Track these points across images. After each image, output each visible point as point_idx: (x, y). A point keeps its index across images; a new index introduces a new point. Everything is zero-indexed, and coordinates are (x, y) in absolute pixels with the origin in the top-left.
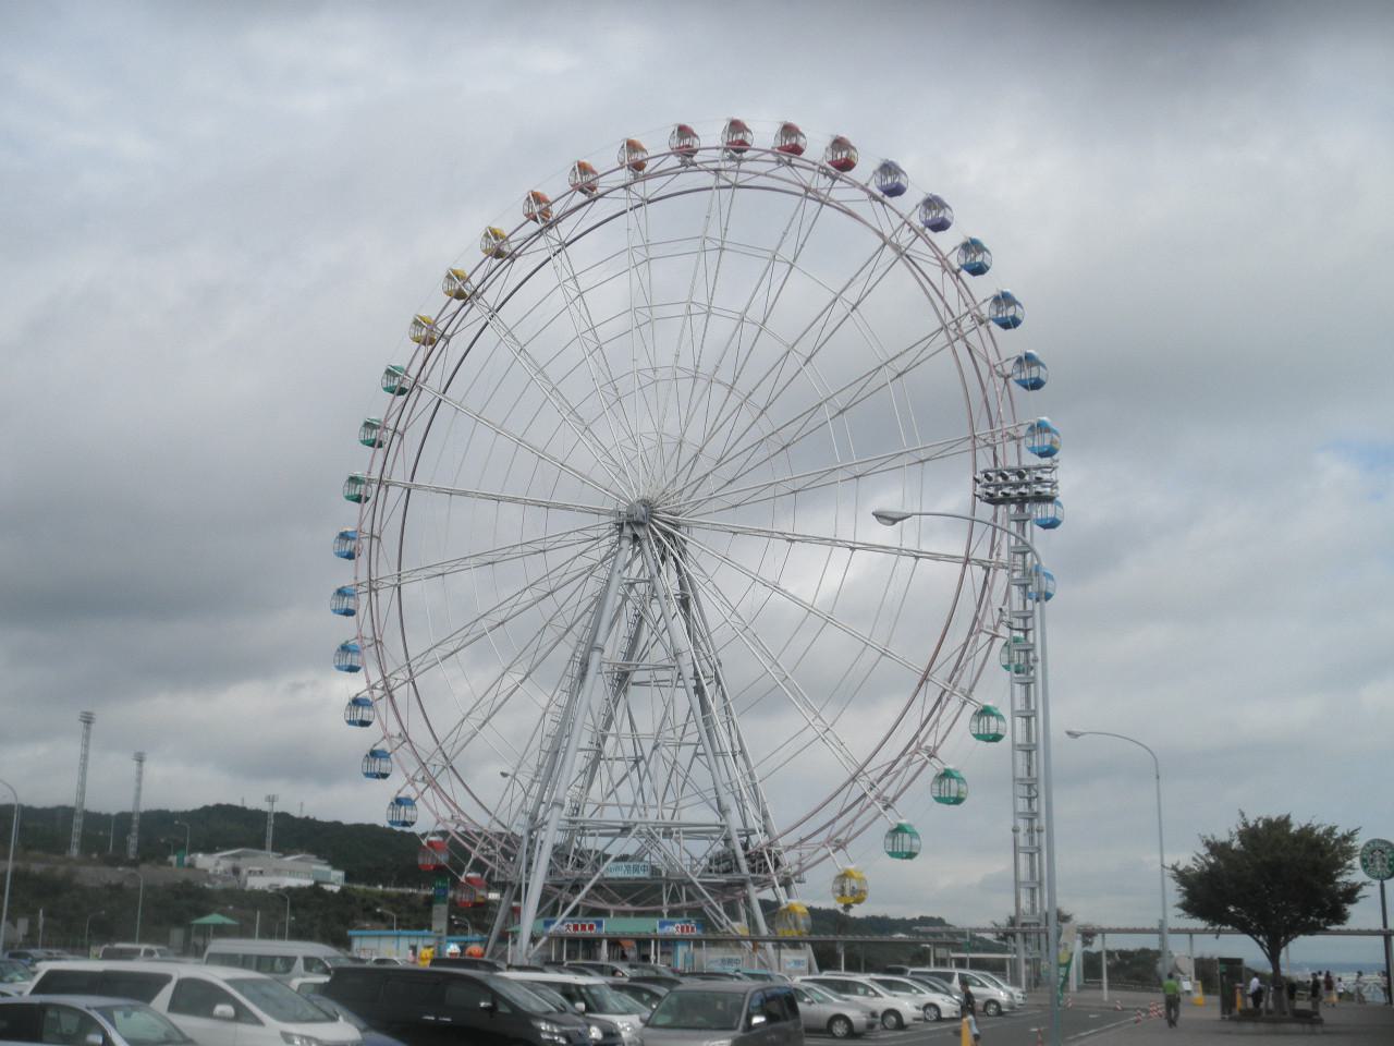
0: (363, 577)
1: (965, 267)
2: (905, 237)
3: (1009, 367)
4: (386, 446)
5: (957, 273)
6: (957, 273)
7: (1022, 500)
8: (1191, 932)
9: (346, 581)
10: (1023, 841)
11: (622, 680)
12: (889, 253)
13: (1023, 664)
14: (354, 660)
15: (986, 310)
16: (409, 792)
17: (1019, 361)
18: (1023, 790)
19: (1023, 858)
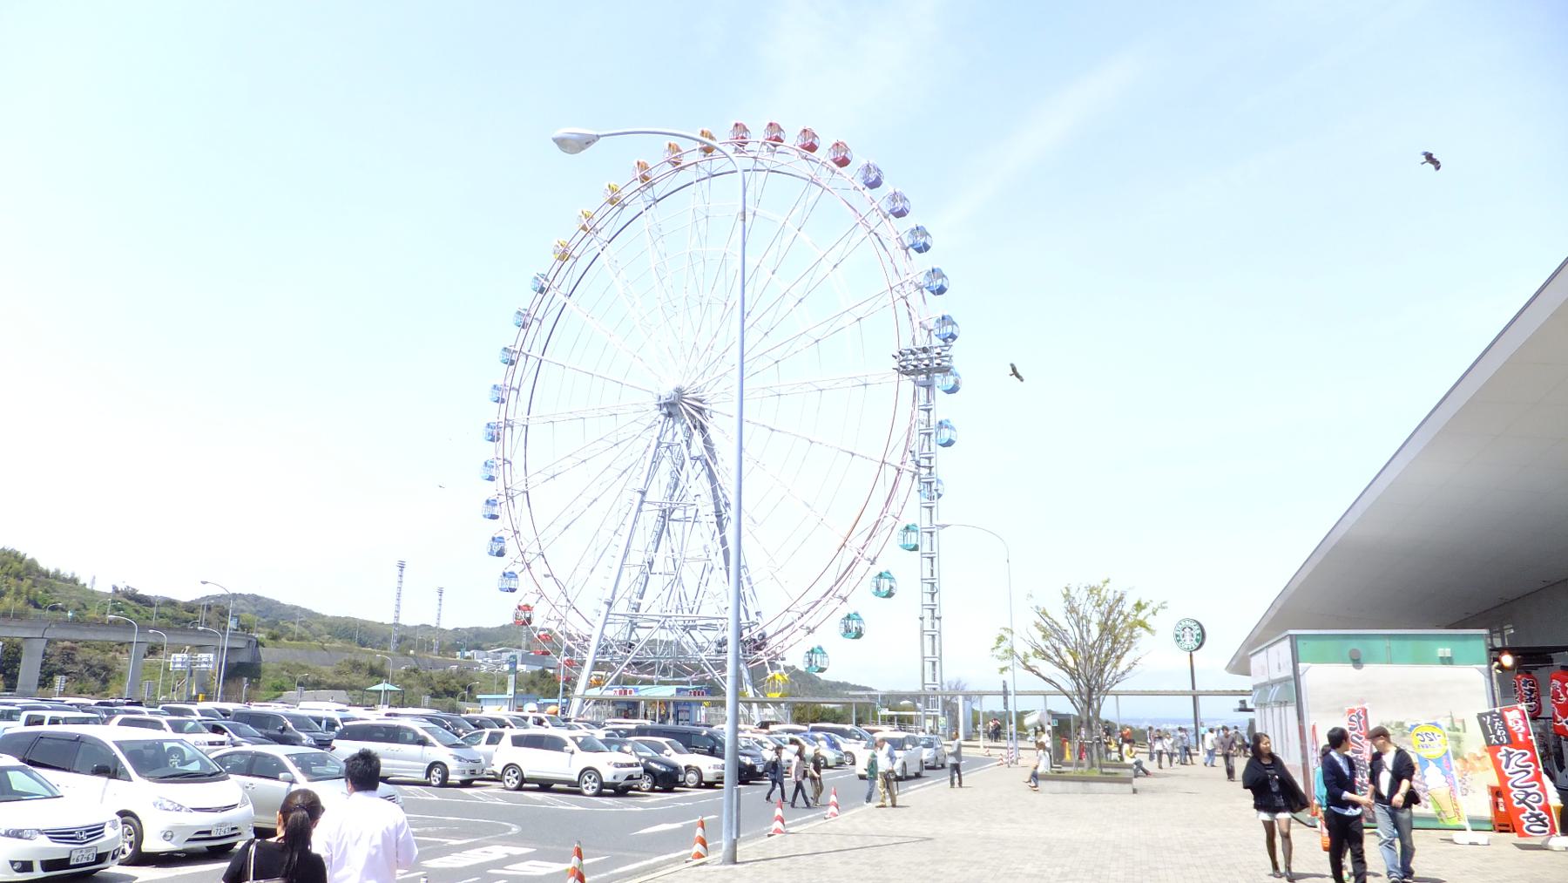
0: (502, 490)
1: (892, 212)
2: (874, 220)
3: (921, 279)
4: (674, 140)
5: (907, 249)
6: (907, 249)
7: (929, 371)
8: (1045, 694)
9: (492, 495)
10: (928, 626)
11: (665, 516)
12: (862, 231)
13: (930, 489)
14: (496, 511)
15: (921, 279)
16: (517, 569)
17: (912, 232)
18: (927, 588)
19: (927, 639)
